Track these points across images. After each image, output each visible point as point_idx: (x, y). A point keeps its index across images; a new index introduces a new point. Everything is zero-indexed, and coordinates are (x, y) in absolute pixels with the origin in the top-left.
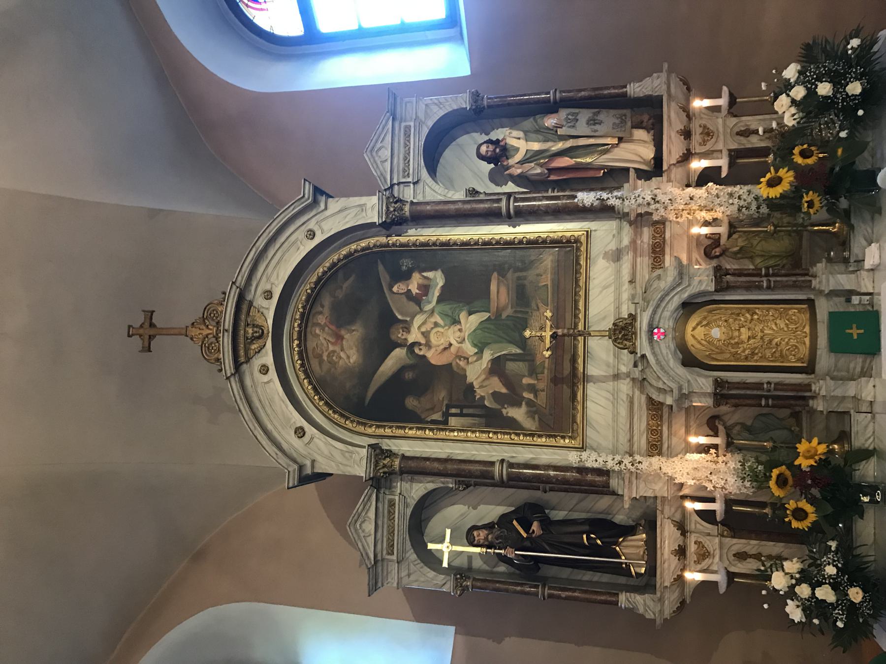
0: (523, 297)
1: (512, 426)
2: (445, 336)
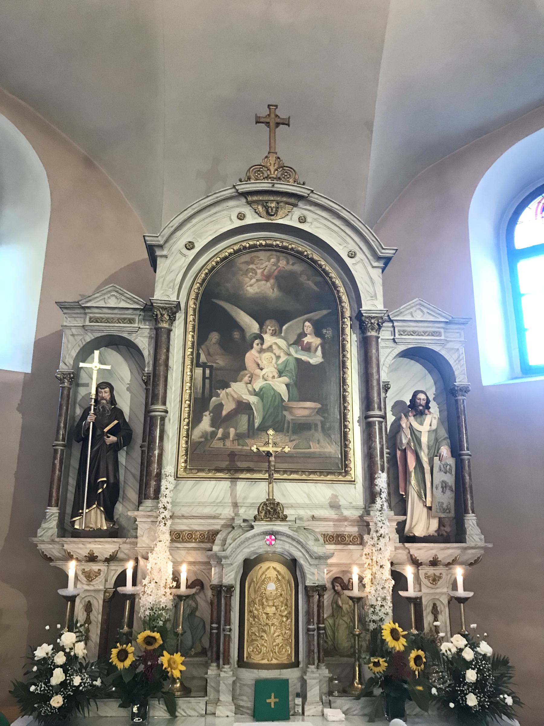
1: (195, 419)
2: (270, 363)
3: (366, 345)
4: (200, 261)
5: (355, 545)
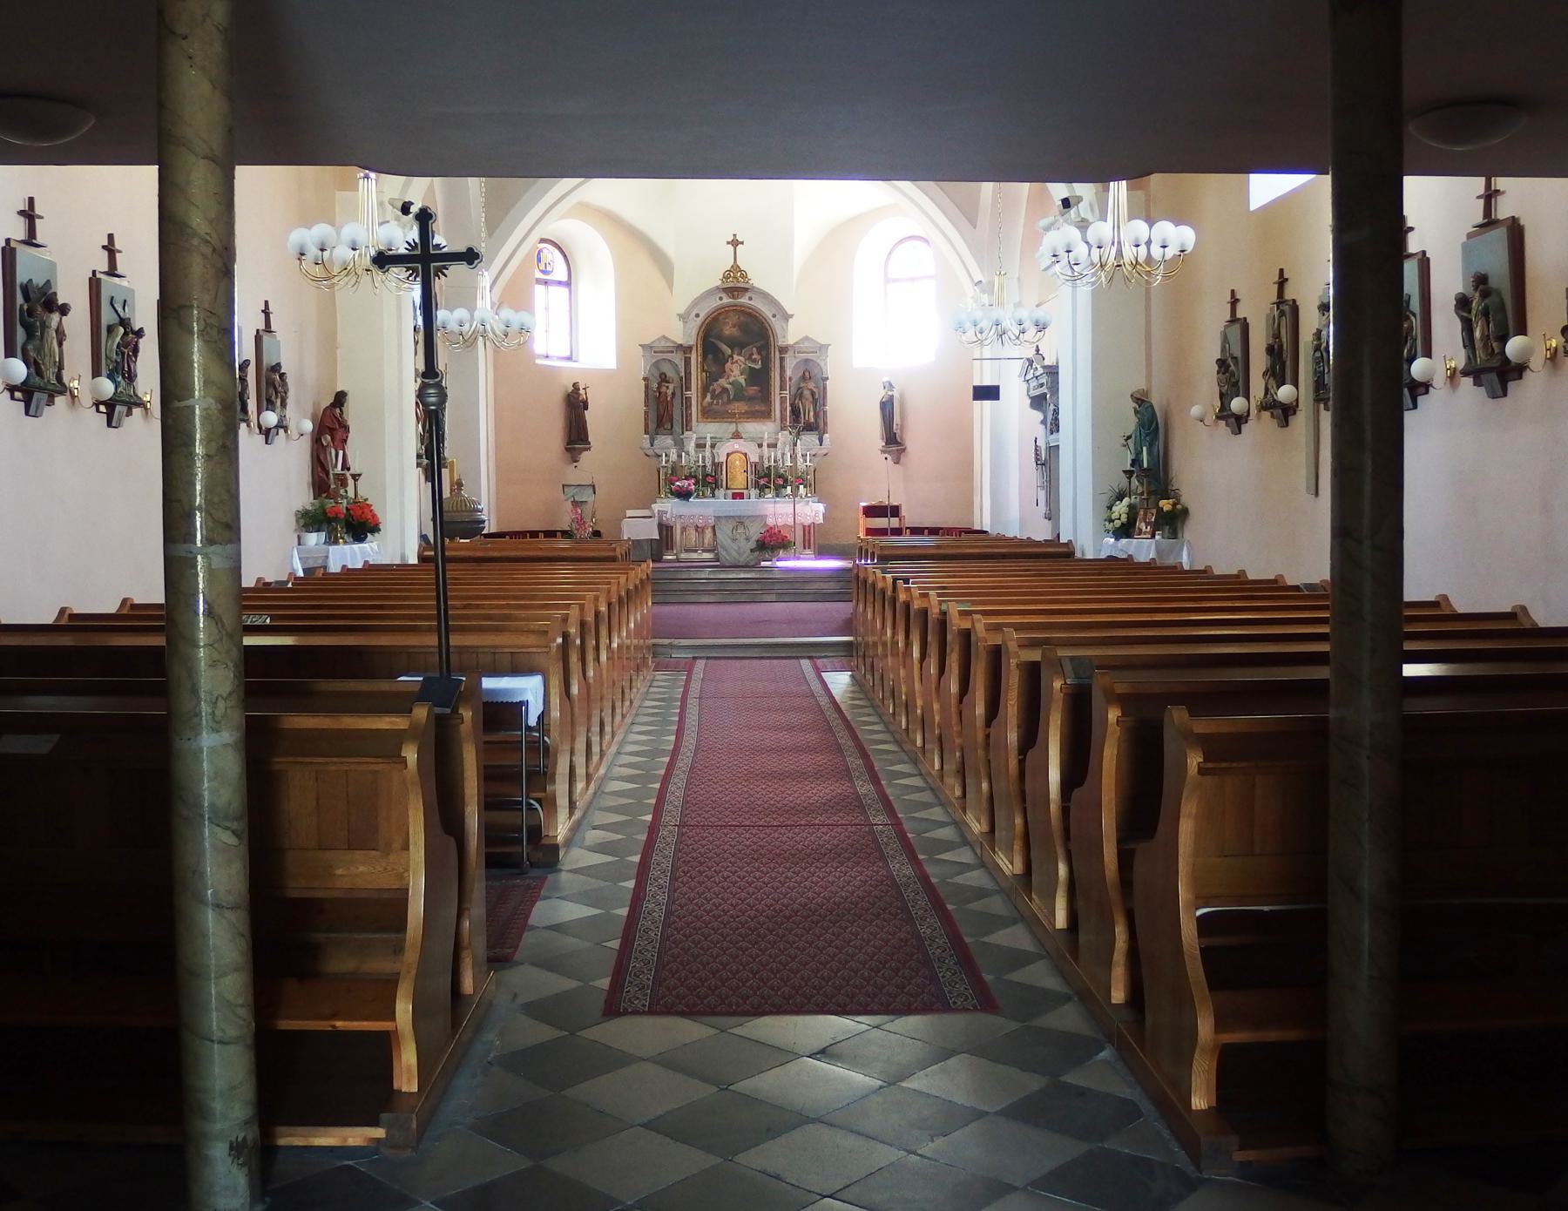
0: (750, 399)
1: (704, 397)
2: (736, 371)
3: (782, 359)
4: (607, 252)
5: (956, 1010)
